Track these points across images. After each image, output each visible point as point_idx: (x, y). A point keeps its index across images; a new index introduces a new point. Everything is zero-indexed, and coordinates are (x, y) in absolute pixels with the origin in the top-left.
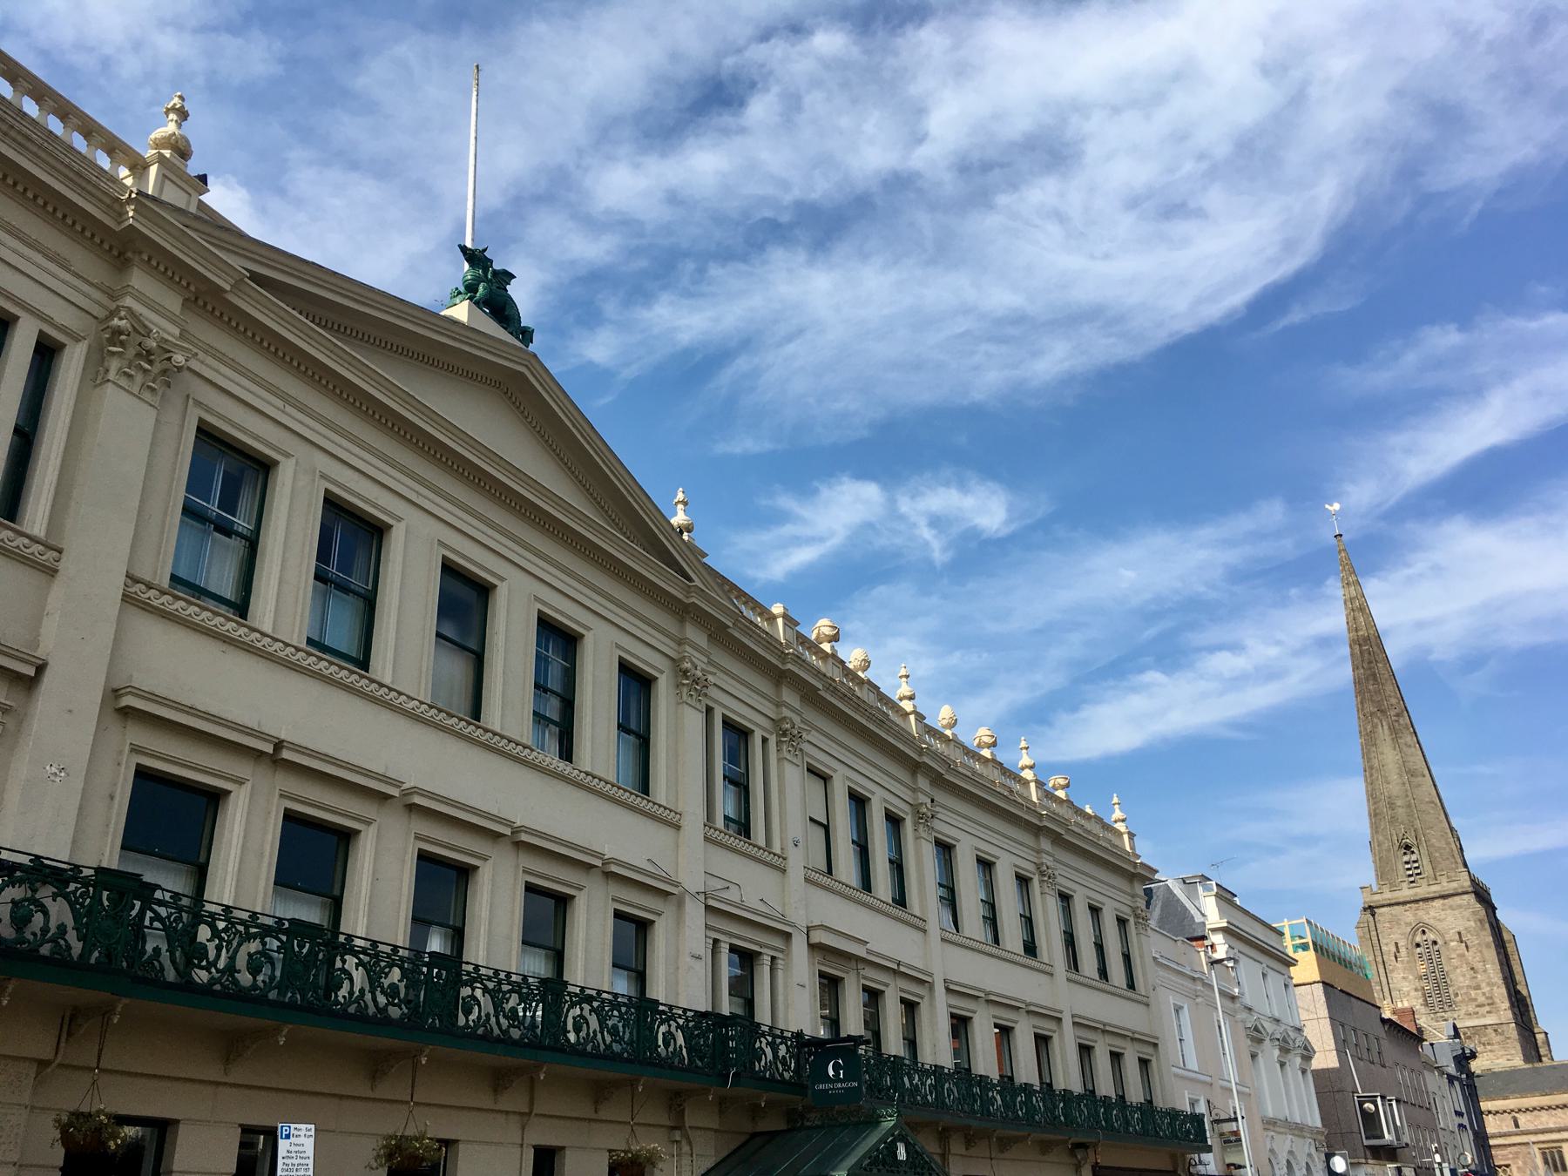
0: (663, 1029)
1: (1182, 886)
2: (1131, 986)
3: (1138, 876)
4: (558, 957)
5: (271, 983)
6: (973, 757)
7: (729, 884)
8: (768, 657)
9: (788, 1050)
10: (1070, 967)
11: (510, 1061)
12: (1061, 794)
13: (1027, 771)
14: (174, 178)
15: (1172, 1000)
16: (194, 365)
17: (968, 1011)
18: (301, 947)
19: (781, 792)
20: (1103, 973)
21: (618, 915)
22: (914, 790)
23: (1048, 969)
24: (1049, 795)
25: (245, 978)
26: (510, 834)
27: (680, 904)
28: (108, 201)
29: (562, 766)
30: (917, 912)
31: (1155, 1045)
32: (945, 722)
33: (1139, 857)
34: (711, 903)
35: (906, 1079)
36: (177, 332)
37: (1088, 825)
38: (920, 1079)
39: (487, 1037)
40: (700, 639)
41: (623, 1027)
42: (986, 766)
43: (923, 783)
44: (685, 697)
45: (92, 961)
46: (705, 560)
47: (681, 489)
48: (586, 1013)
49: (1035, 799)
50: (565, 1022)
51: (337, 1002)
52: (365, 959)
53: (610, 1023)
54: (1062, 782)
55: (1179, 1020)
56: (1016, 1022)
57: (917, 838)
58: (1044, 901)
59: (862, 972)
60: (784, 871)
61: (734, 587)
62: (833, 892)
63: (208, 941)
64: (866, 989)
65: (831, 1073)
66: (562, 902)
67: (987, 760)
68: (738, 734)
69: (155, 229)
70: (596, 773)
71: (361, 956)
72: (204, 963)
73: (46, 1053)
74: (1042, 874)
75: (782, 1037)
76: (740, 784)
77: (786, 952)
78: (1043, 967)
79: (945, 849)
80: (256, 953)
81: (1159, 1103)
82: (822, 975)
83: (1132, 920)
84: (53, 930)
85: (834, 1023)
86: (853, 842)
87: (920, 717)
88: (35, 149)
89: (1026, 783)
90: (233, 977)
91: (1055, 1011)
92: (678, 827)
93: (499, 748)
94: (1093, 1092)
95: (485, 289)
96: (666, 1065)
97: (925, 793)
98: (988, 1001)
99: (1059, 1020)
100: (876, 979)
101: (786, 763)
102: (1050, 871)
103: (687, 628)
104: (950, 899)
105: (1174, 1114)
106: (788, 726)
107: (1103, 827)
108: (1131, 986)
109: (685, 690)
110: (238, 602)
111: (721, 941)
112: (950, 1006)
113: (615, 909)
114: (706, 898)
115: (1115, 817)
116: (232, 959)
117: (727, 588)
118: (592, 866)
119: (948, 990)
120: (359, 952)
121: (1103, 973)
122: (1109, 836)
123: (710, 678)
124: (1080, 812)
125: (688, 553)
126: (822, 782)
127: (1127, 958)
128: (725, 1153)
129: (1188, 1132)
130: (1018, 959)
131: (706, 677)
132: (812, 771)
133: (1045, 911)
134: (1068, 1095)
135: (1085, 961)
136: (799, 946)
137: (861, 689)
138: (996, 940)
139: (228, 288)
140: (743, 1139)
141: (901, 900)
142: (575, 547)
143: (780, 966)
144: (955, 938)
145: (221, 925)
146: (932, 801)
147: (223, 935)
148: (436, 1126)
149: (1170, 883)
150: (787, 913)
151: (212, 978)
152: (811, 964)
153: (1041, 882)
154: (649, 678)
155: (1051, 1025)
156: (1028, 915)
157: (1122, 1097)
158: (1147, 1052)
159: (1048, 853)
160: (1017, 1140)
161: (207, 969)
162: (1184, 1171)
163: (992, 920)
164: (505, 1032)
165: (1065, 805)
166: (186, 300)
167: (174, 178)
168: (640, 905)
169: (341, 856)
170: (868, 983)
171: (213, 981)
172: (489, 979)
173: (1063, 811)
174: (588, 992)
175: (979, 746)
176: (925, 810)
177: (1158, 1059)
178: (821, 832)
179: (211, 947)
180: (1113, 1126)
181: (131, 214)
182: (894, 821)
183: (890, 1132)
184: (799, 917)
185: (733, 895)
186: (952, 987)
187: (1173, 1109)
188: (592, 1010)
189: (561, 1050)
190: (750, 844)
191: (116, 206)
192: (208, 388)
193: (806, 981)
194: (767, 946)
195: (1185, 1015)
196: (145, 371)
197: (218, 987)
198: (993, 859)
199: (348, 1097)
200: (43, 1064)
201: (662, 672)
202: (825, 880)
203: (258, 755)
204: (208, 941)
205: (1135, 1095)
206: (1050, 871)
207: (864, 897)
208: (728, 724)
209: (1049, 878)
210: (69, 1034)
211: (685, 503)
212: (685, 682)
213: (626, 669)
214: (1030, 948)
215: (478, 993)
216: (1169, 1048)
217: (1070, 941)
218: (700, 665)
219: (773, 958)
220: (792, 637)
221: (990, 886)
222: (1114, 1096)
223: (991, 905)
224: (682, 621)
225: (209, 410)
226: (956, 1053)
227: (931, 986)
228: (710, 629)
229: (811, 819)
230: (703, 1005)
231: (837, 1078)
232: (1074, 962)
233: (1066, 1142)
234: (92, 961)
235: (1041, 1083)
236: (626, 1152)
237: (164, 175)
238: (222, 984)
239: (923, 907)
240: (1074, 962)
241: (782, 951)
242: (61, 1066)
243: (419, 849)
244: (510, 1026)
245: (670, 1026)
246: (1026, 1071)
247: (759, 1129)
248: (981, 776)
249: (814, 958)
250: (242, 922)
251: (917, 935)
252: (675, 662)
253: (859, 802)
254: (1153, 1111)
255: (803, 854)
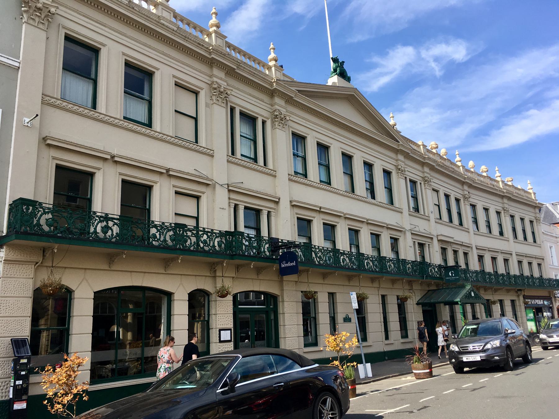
0: (342, 257)
1: (552, 206)
2: (535, 242)
3: (538, 207)
4: (334, 243)
5: (191, 245)
6: (480, 176)
7: (416, 226)
8: (421, 160)
9: (438, 270)
10: (514, 238)
11: (327, 271)
12: (510, 183)
13: (498, 178)
14: (278, 70)
15: (549, 245)
16: (291, 118)
17: (359, 227)
18: (180, 231)
19: (426, 198)
20: (525, 239)
21: (371, 234)
22: (423, 172)
23: (507, 239)
24: (506, 185)
25: (101, 235)
26: (165, 172)
27: (405, 233)
28: (269, 83)
29: (373, 201)
30: (271, 168)
31: (543, 259)
32: (471, 166)
33: (537, 200)
34: (413, 232)
35: (468, 275)
36: (226, 84)
37: (519, 192)
38: (472, 274)
39: (349, 268)
40: (222, 74)
41: (323, 256)
42: (472, 174)
43: (466, 188)
44: (400, 176)
45: (178, 247)
46: (401, 134)
47: (272, 43)
48: (345, 258)
49: (501, 187)
50: (340, 260)
51: (187, 247)
52: (348, 255)
53: (318, 255)
54: (510, 179)
55: (551, 251)
56: (485, 254)
57: (465, 205)
58: (505, 219)
59: (452, 246)
60: (429, 220)
61: (408, 139)
62: (442, 224)
63: (156, 233)
64: (453, 250)
65: (450, 275)
66: (333, 227)
67: (485, 177)
68: (413, 183)
69: (279, 87)
70: (382, 202)
71: (193, 231)
72: (156, 239)
73: (297, 280)
74: (504, 210)
75: (436, 266)
76: (415, 198)
77: (432, 243)
78: (506, 239)
79: (473, 206)
80: (172, 235)
81: (545, 276)
82: (442, 248)
83: (535, 221)
84: (193, 243)
85: (445, 261)
86: (385, 188)
87: (424, 146)
88: (243, 69)
89: (498, 182)
90: (96, 235)
91: (510, 251)
92: (402, 213)
93: (360, 199)
94: (522, 274)
95: (339, 69)
96: (370, 271)
97: (467, 191)
98: (489, 251)
99: (511, 254)
100: (456, 247)
101: (427, 189)
102: (507, 209)
103: (214, 70)
104: (476, 221)
105: (550, 280)
106: (427, 179)
107: (525, 192)
108: (535, 242)
109: (400, 174)
110: (148, 123)
111: (239, 205)
112: (477, 253)
113: (349, 228)
114: (228, 187)
115: (528, 188)
116: (326, 258)
117: (406, 140)
118: (341, 216)
119: (477, 248)
120: (192, 230)
121: (525, 239)
122: (527, 195)
123: (406, 169)
124: (516, 188)
125: (396, 132)
126: (195, 95)
127: (533, 233)
128: (422, 296)
129: (554, 285)
130: (498, 237)
131: (226, 92)
132: (434, 190)
133: (506, 222)
134: (503, 275)
135: (519, 235)
136: (435, 241)
137: (445, 162)
138: (490, 232)
139: (294, 96)
140: (426, 292)
141: (461, 224)
142: (263, 91)
143: (272, 215)
144: (478, 233)
145: (323, 251)
146: (469, 193)
147: (161, 231)
148: (313, 289)
149: (548, 205)
150: (431, 232)
151: (209, 249)
152: (439, 245)
153: (504, 213)
154: (255, 118)
155: (509, 256)
156: (500, 223)
157: (532, 276)
158: (540, 261)
159: (506, 204)
160: (500, 289)
161: (157, 241)
162: (553, 296)
163: (489, 226)
164: (375, 270)
165: (511, 187)
166: (285, 102)
167: (278, 70)
168: (395, 234)
169: (309, 227)
170: (454, 249)
171: (210, 250)
172: (371, 258)
173: (511, 189)
174: (391, 259)
175: (482, 172)
176: (467, 196)
177: (544, 263)
178: (437, 207)
179: (158, 235)
180: (530, 284)
181: (275, 85)
182: (458, 200)
183: (470, 289)
184: (434, 233)
185: (417, 229)
186: (478, 247)
187: (550, 278)
188: (392, 263)
189: (186, 251)
190: (331, 187)
191: (271, 84)
192: (237, 99)
193: (438, 250)
194: (240, 201)
195: (553, 249)
196: (221, 98)
197: (211, 251)
198: (475, 204)
199: (68, 268)
200: (296, 282)
201: (393, 170)
202: (440, 221)
203: (316, 211)
204: (156, 233)
205: (536, 274)
206: (507, 209)
207: (451, 225)
208: (411, 181)
209: (507, 211)
210: (238, 271)
211: (274, 49)
212: (399, 172)
213: (366, 163)
214: (501, 233)
215: (369, 261)
216: (548, 260)
217: (514, 230)
218: (403, 166)
219: (429, 245)
220: (426, 151)
221: (487, 216)
222: (530, 275)
223: (488, 222)
224: (397, 154)
225: (293, 128)
226: (480, 266)
227: (472, 248)
228: (286, 99)
229: (435, 204)
230: (414, 260)
231: (452, 276)
232: (516, 237)
233: (515, 289)
234: (178, 247)
235: (494, 272)
236: (404, 296)
237: (276, 70)
238: (92, 238)
239: (468, 224)
240: (516, 237)
241: (274, 209)
242: (299, 282)
243: (122, 179)
244: (320, 260)
245: (344, 257)
246: (501, 270)
247: (430, 289)
248: (483, 182)
249: (439, 243)
250: (326, 250)
251: (467, 233)
252: (396, 166)
253: (447, 196)
254: (542, 279)
255: (434, 216)
